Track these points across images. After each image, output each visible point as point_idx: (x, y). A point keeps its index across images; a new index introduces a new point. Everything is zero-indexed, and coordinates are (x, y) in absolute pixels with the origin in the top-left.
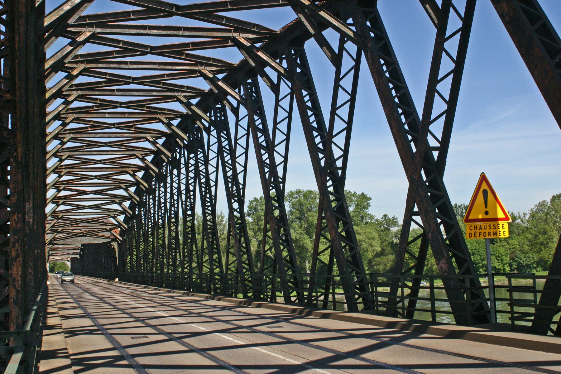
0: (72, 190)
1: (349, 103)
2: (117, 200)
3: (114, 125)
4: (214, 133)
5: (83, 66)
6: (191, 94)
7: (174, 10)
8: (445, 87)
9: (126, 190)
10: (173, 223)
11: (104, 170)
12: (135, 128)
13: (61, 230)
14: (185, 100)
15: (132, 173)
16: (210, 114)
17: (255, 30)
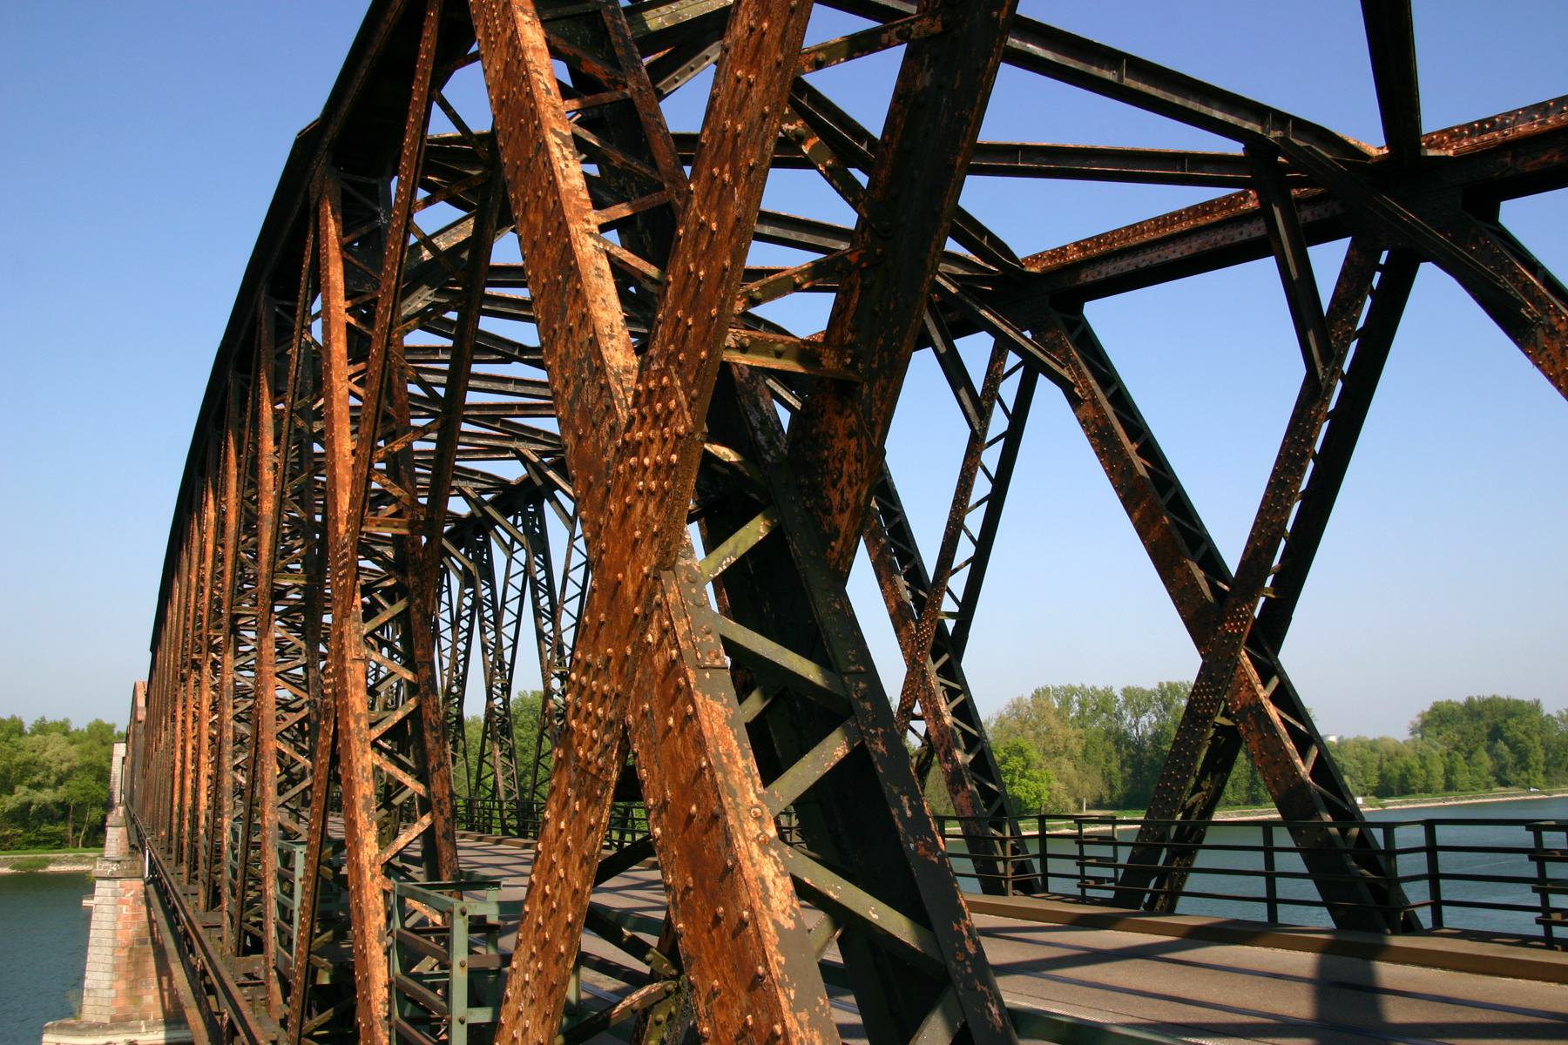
4: (521, 556)
7: (516, 353)
8: (974, 521)
14: (474, 496)
16: (515, 521)
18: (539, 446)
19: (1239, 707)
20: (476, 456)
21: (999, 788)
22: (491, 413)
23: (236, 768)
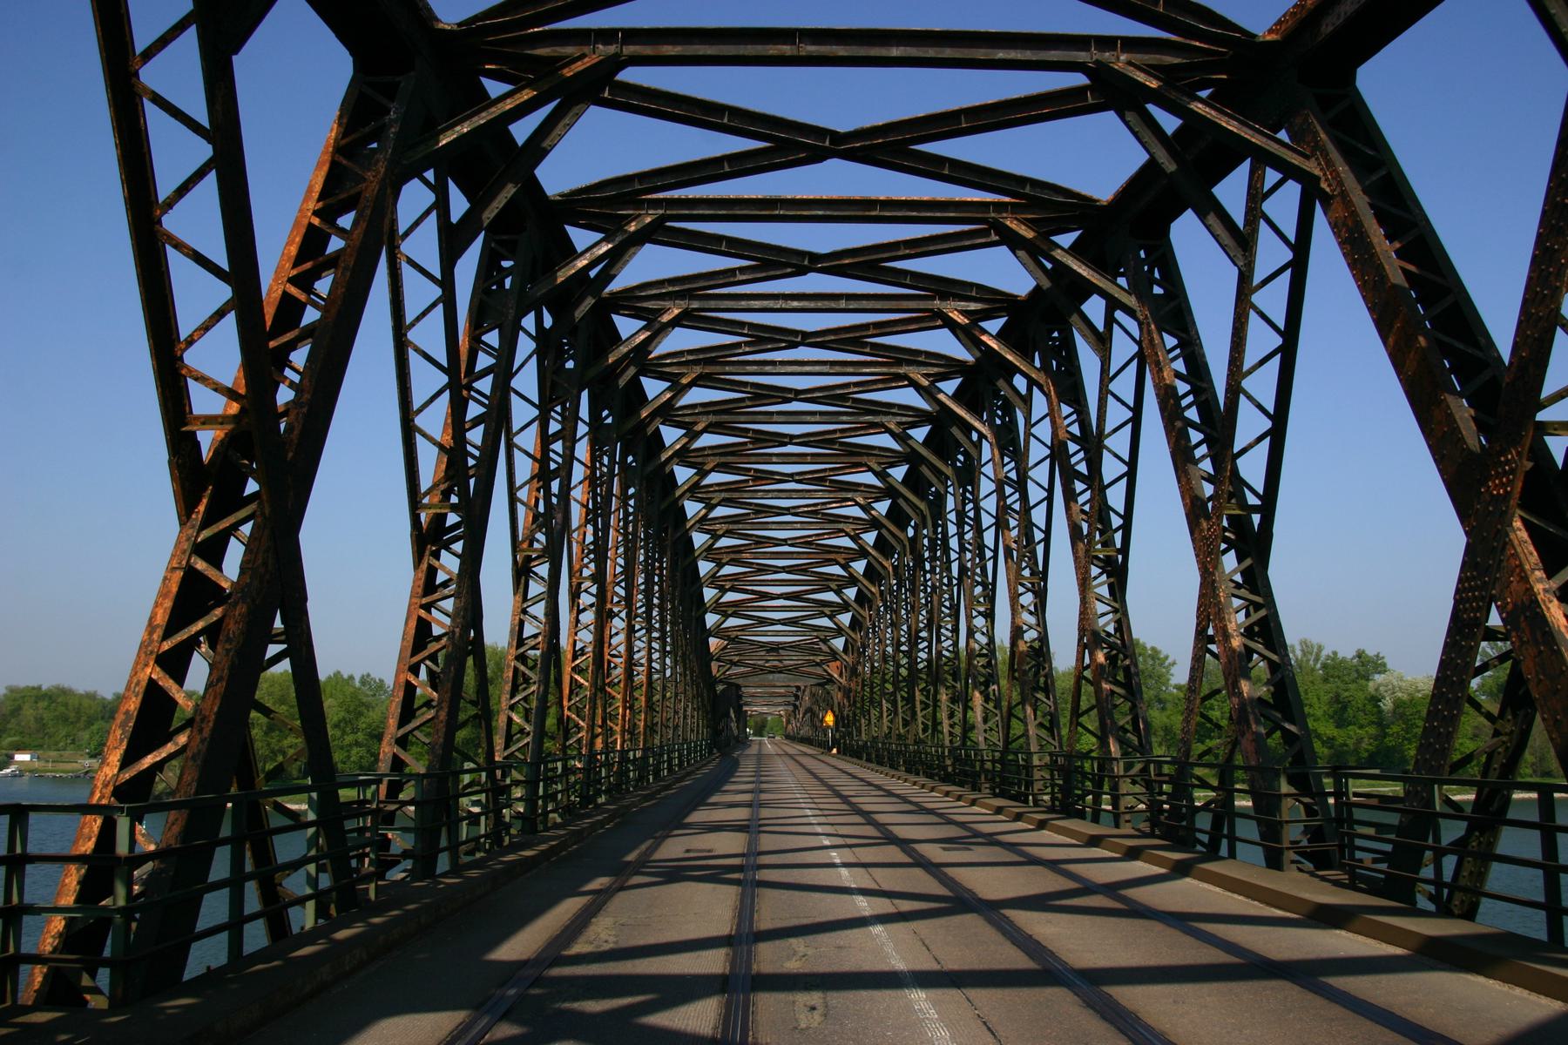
0: (746, 592)
1: (1130, 425)
2: (827, 610)
3: (791, 477)
5: (698, 370)
6: (910, 419)
7: (806, 263)
9: (838, 592)
10: (903, 652)
11: (795, 556)
12: (831, 481)
13: (738, 661)
15: (843, 562)
17: (974, 294)
18: (930, 368)
19: (1510, 607)
20: (875, 387)
21: (1300, 730)
22: (851, 335)
23: (512, 708)
